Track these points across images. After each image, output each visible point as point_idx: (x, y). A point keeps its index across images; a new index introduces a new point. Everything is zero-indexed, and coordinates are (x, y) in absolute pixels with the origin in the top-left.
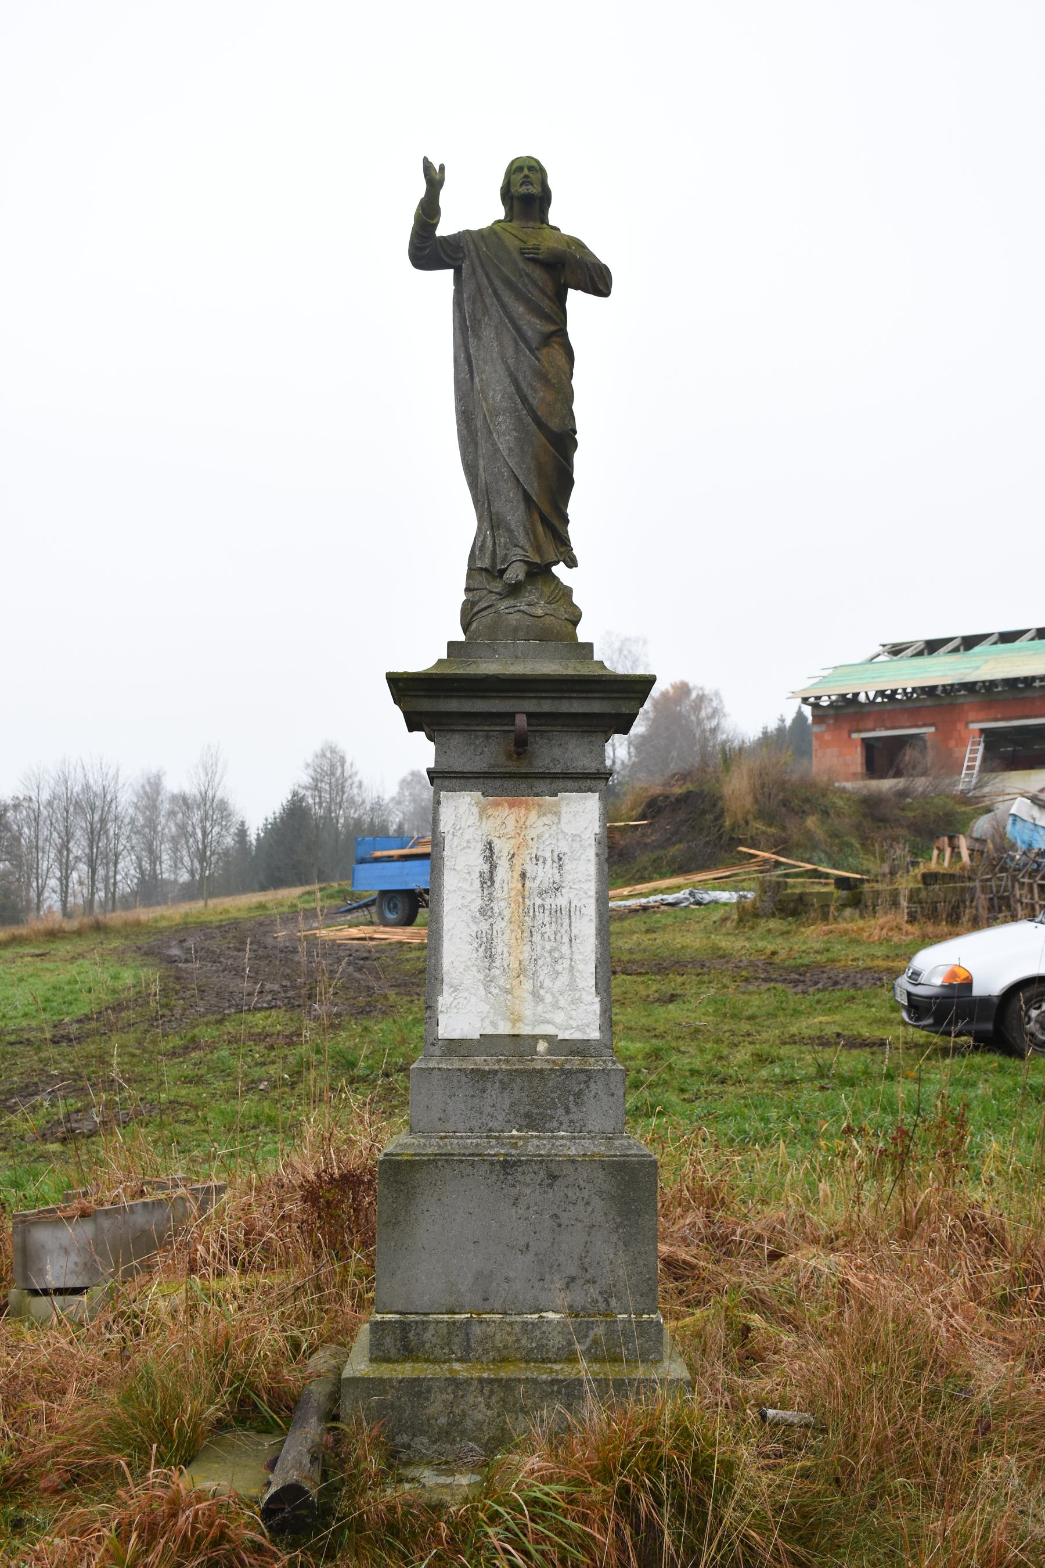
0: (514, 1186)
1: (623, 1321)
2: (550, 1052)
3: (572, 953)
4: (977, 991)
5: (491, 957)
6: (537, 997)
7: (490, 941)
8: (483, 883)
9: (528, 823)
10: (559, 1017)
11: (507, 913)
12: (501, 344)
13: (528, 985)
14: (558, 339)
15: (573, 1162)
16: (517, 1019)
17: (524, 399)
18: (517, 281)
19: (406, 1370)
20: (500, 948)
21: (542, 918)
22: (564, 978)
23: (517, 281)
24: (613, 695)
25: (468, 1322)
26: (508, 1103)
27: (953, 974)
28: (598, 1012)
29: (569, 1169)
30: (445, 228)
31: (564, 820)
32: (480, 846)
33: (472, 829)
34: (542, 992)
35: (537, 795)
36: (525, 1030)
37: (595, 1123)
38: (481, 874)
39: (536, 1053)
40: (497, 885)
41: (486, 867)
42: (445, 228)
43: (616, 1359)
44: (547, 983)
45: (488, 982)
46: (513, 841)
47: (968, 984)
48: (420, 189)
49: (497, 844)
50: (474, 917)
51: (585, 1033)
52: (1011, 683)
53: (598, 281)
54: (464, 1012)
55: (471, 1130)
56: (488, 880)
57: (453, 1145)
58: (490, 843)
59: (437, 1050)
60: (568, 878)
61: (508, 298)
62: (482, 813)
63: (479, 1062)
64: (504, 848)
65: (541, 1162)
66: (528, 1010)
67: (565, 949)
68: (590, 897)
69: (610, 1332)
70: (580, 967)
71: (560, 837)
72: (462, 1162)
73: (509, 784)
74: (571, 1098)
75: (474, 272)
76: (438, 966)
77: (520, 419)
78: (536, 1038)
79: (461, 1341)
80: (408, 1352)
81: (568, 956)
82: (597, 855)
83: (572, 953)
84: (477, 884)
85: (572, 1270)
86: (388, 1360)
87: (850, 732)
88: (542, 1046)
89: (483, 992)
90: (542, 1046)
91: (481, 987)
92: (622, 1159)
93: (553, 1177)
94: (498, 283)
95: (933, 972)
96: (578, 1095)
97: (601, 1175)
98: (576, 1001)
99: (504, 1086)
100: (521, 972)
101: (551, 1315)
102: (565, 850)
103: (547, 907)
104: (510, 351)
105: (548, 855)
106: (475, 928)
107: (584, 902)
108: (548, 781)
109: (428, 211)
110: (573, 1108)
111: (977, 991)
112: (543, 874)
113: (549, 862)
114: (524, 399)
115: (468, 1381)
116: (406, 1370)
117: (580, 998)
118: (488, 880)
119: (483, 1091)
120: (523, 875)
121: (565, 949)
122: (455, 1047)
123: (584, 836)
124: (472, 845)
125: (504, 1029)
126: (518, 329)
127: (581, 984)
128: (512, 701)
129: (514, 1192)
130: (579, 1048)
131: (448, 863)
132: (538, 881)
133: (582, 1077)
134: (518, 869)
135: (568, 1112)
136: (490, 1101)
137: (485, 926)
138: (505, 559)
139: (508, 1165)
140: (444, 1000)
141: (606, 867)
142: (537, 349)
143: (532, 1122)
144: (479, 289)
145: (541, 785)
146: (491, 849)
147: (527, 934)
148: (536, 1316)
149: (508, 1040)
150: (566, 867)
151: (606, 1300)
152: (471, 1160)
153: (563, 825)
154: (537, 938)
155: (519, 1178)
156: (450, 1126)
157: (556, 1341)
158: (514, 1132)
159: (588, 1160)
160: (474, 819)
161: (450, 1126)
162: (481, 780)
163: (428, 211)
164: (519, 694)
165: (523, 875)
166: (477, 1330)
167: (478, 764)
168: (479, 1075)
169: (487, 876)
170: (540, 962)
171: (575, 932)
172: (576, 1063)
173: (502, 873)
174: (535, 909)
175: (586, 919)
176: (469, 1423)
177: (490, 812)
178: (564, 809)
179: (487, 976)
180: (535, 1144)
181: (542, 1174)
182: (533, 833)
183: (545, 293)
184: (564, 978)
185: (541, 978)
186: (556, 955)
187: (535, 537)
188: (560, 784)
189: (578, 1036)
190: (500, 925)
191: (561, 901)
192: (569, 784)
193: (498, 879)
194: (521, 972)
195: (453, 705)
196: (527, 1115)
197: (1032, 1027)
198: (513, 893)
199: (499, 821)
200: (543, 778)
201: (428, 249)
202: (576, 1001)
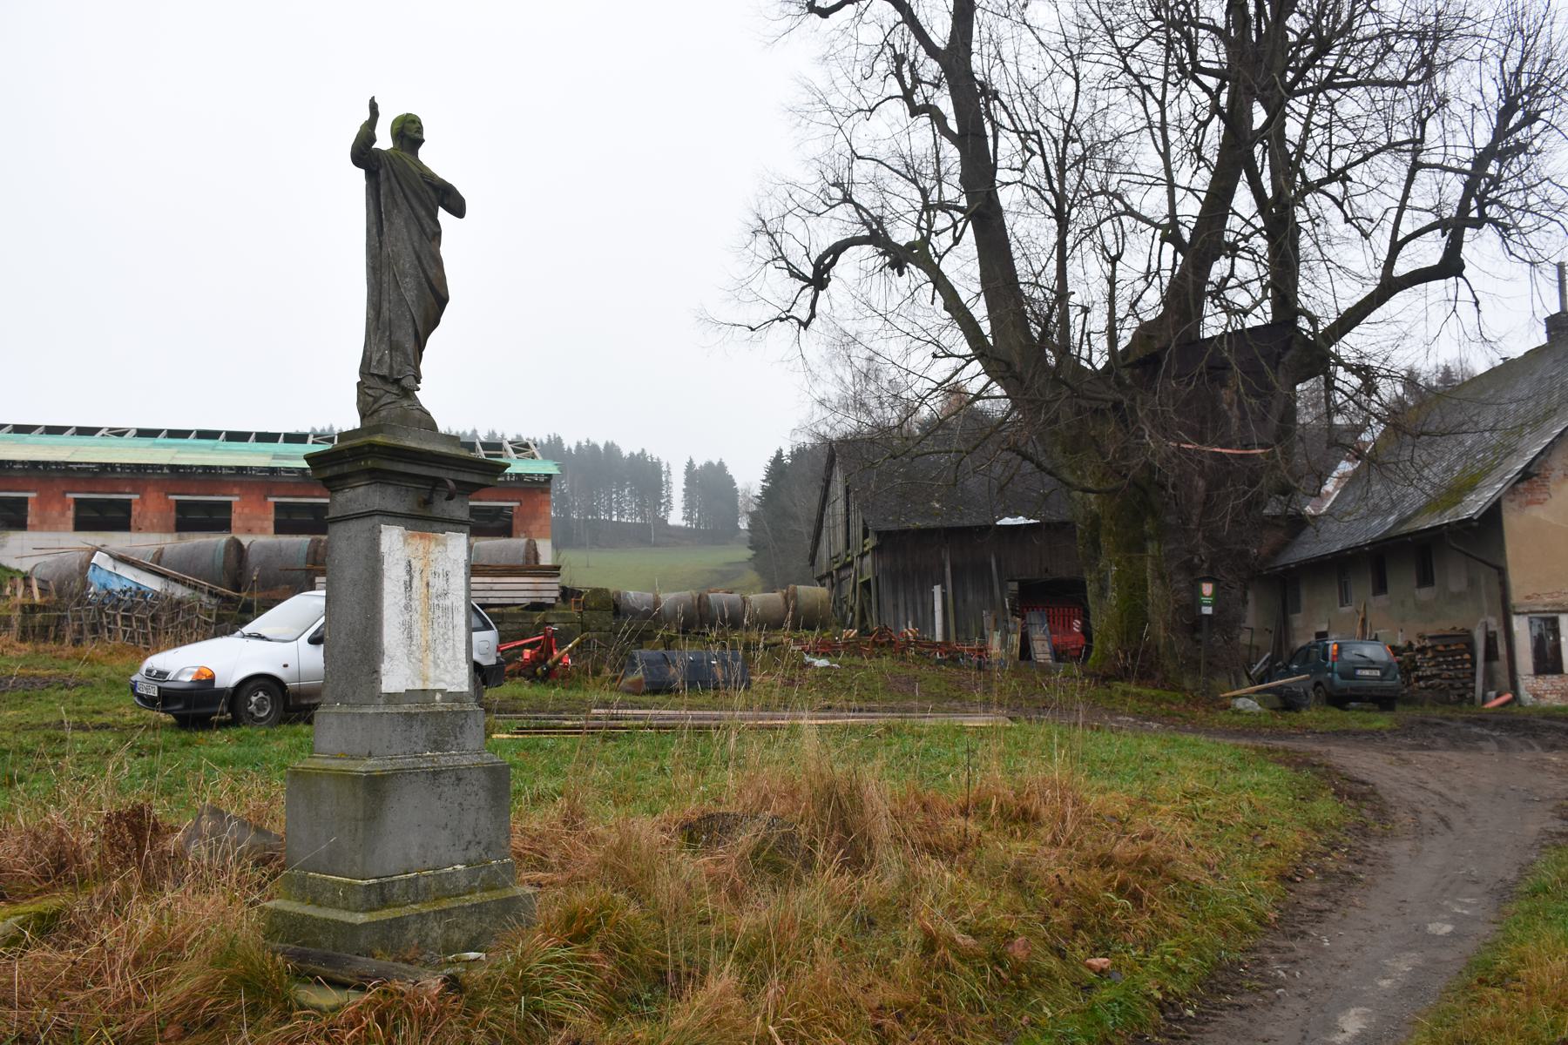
2: (443, 700)
4: (218, 685)
6: (437, 666)
7: (410, 627)
10: (448, 678)
12: (409, 232)
13: (431, 657)
16: (425, 680)
17: (424, 271)
19: (386, 914)
20: (416, 632)
21: (439, 613)
22: (450, 652)
23: (404, 193)
25: (417, 878)
27: (199, 673)
29: (467, 774)
32: (405, 563)
36: (431, 687)
37: (470, 745)
43: (492, 888)
45: (410, 654)
47: (212, 679)
48: (366, 116)
49: (414, 563)
52: (207, 469)
53: (457, 207)
54: (396, 677)
56: (409, 586)
57: (399, 764)
59: (381, 701)
61: (414, 202)
62: (405, 540)
63: (405, 708)
66: (431, 673)
73: (420, 523)
75: (388, 179)
76: (380, 643)
77: (420, 284)
78: (435, 691)
79: (416, 891)
80: (384, 902)
85: (469, 837)
86: (373, 910)
87: (167, 494)
88: (438, 696)
90: (438, 696)
93: (459, 779)
94: (408, 192)
95: (181, 672)
96: (461, 727)
99: (423, 723)
100: (428, 648)
101: (459, 867)
104: (416, 238)
111: (218, 685)
112: (438, 584)
114: (424, 271)
115: (428, 914)
116: (386, 914)
118: (409, 586)
122: (392, 698)
125: (419, 686)
126: (421, 225)
130: (457, 697)
131: (386, 574)
138: (399, 372)
139: (436, 774)
140: (385, 667)
143: (438, 746)
144: (391, 190)
145: (437, 526)
152: (414, 772)
156: (393, 751)
157: (463, 882)
161: (393, 751)
167: (402, 509)
168: (409, 716)
172: (457, 707)
173: (416, 583)
174: (433, 607)
176: (429, 940)
180: (444, 760)
182: (432, 557)
184: (450, 652)
188: (446, 526)
189: (457, 689)
191: (448, 602)
194: (428, 648)
195: (401, 467)
196: (435, 742)
197: (252, 708)
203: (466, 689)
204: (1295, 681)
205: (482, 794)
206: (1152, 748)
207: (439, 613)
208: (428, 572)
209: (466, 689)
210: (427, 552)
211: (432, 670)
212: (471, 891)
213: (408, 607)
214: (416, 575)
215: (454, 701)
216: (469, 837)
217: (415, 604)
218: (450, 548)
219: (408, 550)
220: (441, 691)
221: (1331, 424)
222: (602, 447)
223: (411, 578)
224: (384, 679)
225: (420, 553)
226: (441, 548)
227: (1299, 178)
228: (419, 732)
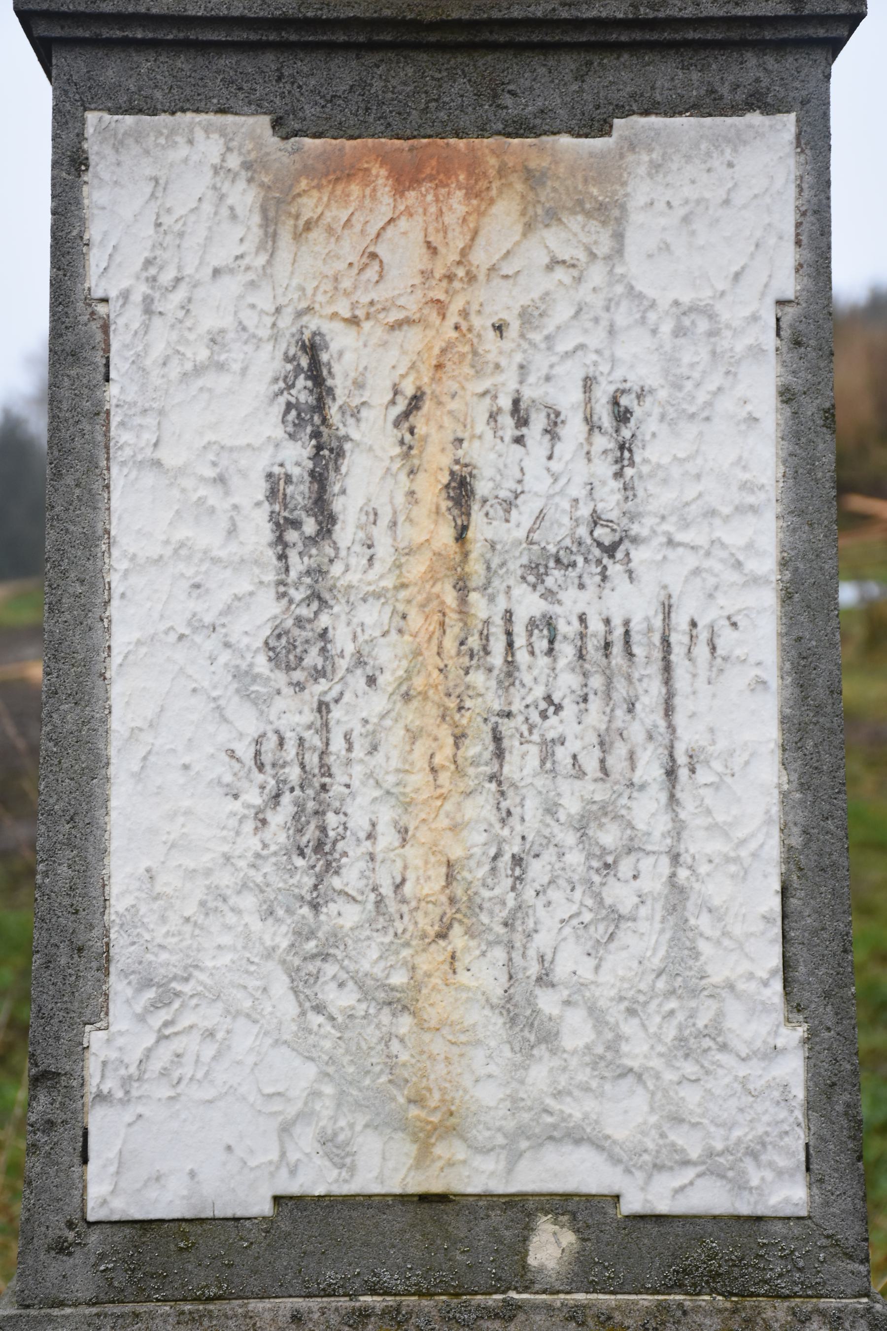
2: (585, 1272)
7: (318, 780)
10: (626, 1115)
13: (485, 973)
16: (438, 1126)
20: (361, 808)
32: (268, 362)
36: (478, 1174)
45: (310, 960)
56: (306, 510)
62: (277, 211)
66: (485, 1080)
73: (396, 76)
76: (85, 892)
78: (522, 1209)
88: (550, 1247)
90: (550, 1247)
100: (457, 912)
112: (549, 484)
118: (306, 510)
125: (382, 1167)
140: (113, 1046)
145: (540, 83)
173: (366, 480)
182: (501, 301)
188: (620, 75)
189: (709, 1198)
191: (629, 601)
194: (457, 912)
204: (331, 1070)
209: (787, 1193)
218: (644, 229)
219: (302, 269)
220: (568, 1206)
222: (781, 523)
223: (327, 455)
224: (104, 1128)
226: (564, 239)
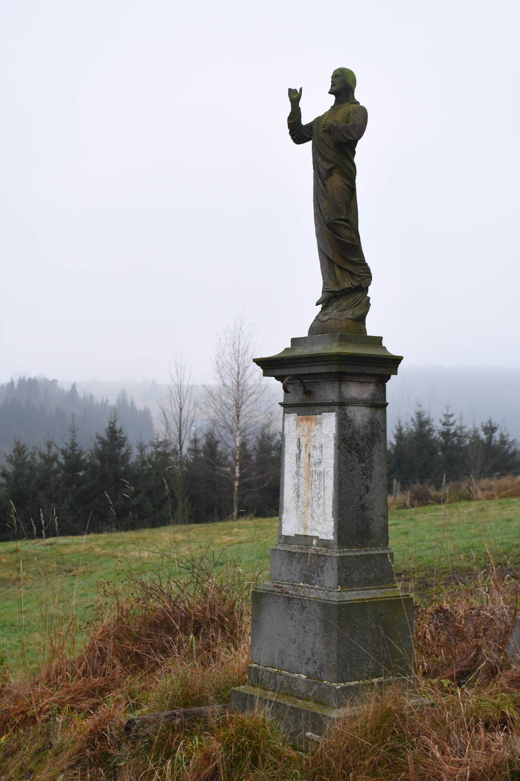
0: (291, 610)
1: (326, 685)
2: (317, 545)
3: (324, 496)
5: (298, 496)
6: (313, 518)
8: (297, 459)
9: (312, 429)
10: (319, 528)
11: (304, 474)
13: (310, 511)
14: (336, 171)
15: (310, 600)
16: (306, 528)
18: (334, 140)
20: (301, 492)
23: (334, 140)
24: (327, 363)
25: (275, 673)
26: (299, 569)
28: (333, 526)
30: (306, 120)
31: (323, 427)
32: (296, 441)
33: (294, 432)
34: (314, 514)
35: (316, 414)
36: (309, 534)
38: (296, 454)
39: (312, 545)
40: (301, 460)
41: (298, 451)
42: (306, 120)
44: (316, 510)
45: (298, 508)
46: (306, 438)
50: (293, 476)
51: (328, 536)
55: (288, 581)
58: (299, 439)
60: (324, 456)
62: (298, 425)
64: (303, 441)
65: (300, 599)
66: (310, 523)
67: (322, 492)
68: (331, 466)
69: (320, 689)
70: (327, 502)
71: (322, 436)
72: (275, 595)
73: (306, 409)
74: (320, 569)
81: (323, 497)
82: (335, 445)
83: (324, 496)
84: (295, 460)
85: (309, 655)
88: (315, 542)
89: (296, 514)
90: (315, 542)
91: (295, 511)
92: (326, 602)
96: (322, 567)
97: (318, 608)
98: (325, 520)
102: (323, 442)
103: (317, 471)
105: (317, 445)
106: (294, 481)
107: (329, 469)
108: (319, 407)
109: (295, 115)
110: (320, 575)
112: (316, 454)
113: (318, 449)
117: (326, 519)
118: (298, 458)
119: (292, 562)
120: (309, 455)
121: (322, 492)
123: (330, 435)
124: (294, 440)
125: (302, 532)
127: (327, 511)
128: (336, 363)
129: (291, 612)
130: (325, 544)
132: (314, 459)
133: (323, 559)
134: (308, 452)
135: (319, 576)
136: (293, 568)
137: (297, 481)
141: (337, 450)
142: (325, 179)
143: (308, 580)
145: (317, 409)
146: (299, 442)
147: (310, 485)
148: (298, 675)
149: (304, 537)
150: (323, 451)
151: (320, 673)
153: (323, 430)
154: (313, 487)
155: (293, 606)
158: (302, 584)
159: (316, 601)
160: (294, 427)
162: (298, 408)
163: (295, 115)
164: (297, 365)
165: (309, 455)
166: (278, 677)
168: (291, 554)
169: (298, 455)
170: (314, 499)
171: (326, 484)
175: (329, 478)
177: (299, 423)
178: (324, 421)
179: (297, 505)
181: (300, 606)
182: (313, 434)
183: (329, 147)
184: (321, 508)
185: (314, 507)
186: (319, 496)
187: (335, 276)
188: (323, 408)
189: (325, 538)
190: (302, 480)
191: (321, 469)
192: (326, 408)
193: (301, 457)
194: (308, 504)
198: (306, 464)
199: (302, 428)
200: (315, 406)
201: (298, 132)
202: (325, 520)
203: (331, 537)
205: (318, 623)
206: (180, 537)
207: (316, 477)
208: (310, 446)
210: (310, 431)
211: (310, 521)
212: (307, 699)
213: (297, 473)
214: (303, 449)
215: (324, 546)
216: (309, 655)
217: (302, 470)
218: (324, 425)
219: (300, 429)
220: (317, 538)
221: (238, 459)
223: (300, 451)
225: (305, 433)
226: (317, 427)
227: (159, 460)
228: (296, 567)
